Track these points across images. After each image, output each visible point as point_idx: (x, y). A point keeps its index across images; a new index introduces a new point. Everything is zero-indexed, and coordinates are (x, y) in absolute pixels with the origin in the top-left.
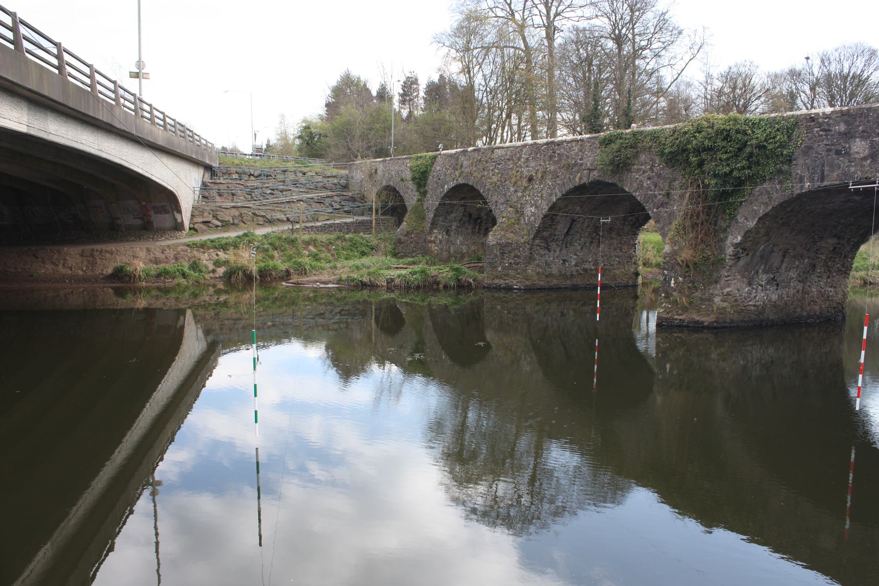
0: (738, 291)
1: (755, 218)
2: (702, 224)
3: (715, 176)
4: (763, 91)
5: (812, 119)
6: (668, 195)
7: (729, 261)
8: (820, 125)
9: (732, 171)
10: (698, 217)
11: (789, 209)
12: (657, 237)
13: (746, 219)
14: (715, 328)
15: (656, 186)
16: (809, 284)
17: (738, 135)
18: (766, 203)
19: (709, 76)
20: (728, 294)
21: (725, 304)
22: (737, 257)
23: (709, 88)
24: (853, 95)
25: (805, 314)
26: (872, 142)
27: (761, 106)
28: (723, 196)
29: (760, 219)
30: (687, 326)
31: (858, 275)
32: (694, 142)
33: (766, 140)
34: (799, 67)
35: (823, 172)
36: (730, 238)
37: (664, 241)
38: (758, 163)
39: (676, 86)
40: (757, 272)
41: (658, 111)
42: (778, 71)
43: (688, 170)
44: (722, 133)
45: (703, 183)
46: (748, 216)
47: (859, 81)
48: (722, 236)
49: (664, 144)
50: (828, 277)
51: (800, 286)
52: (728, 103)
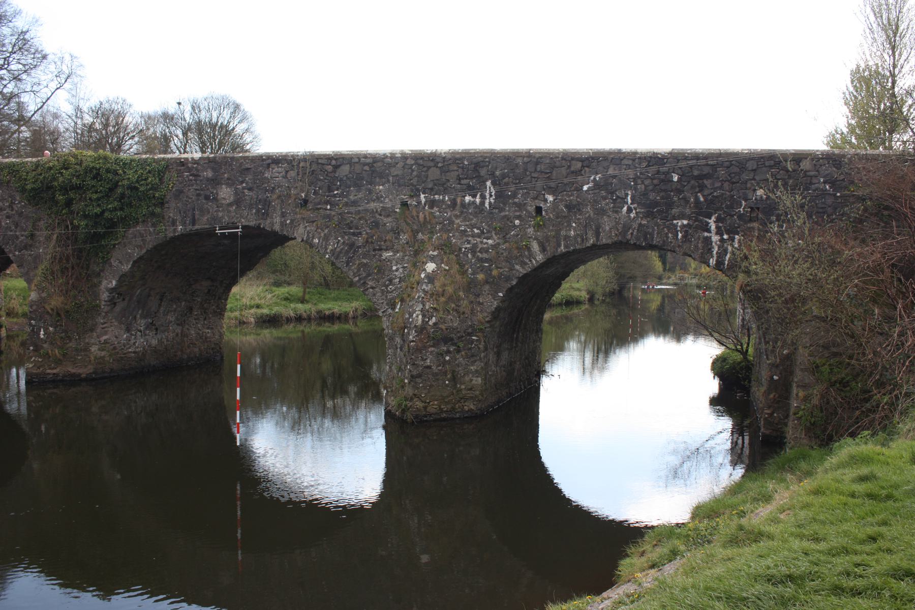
0: (116, 338)
1: (129, 261)
2: (73, 268)
3: (85, 216)
4: (137, 131)
5: (182, 163)
6: (32, 236)
7: (104, 307)
8: (189, 170)
9: (103, 212)
10: (68, 260)
11: (163, 252)
12: (21, 283)
13: (120, 262)
14: (93, 379)
15: (17, 225)
16: (187, 326)
17: (109, 175)
18: (140, 246)
19: (78, 109)
20: (106, 342)
21: (103, 353)
22: (112, 303)
23: (79, 122)
24: (221, 144)
25: (185, 356)
26: (236, 189)
27: (135, 147)
28: (95, 238)
29: (135, 262)
30: (62, 381)
31: (233, 315)
32: (61, 179)
33: (137, 182)
34: (171, 111)
35: (194, 215)
36: (104, 283)
37: (30, 289)
38: (130, 205)
39: (41, 116)
40: (135, 318)
41: (19, 142)
42: (152, 112)
43: (54, 209)
44: (91, 171)
45: (72, 223)
46: (122, 260)
47: (226, 131)
48: (95, 280)
49: (25, 180)
50: (205, 319)
51: (179, 330)
52: (100, 140)
